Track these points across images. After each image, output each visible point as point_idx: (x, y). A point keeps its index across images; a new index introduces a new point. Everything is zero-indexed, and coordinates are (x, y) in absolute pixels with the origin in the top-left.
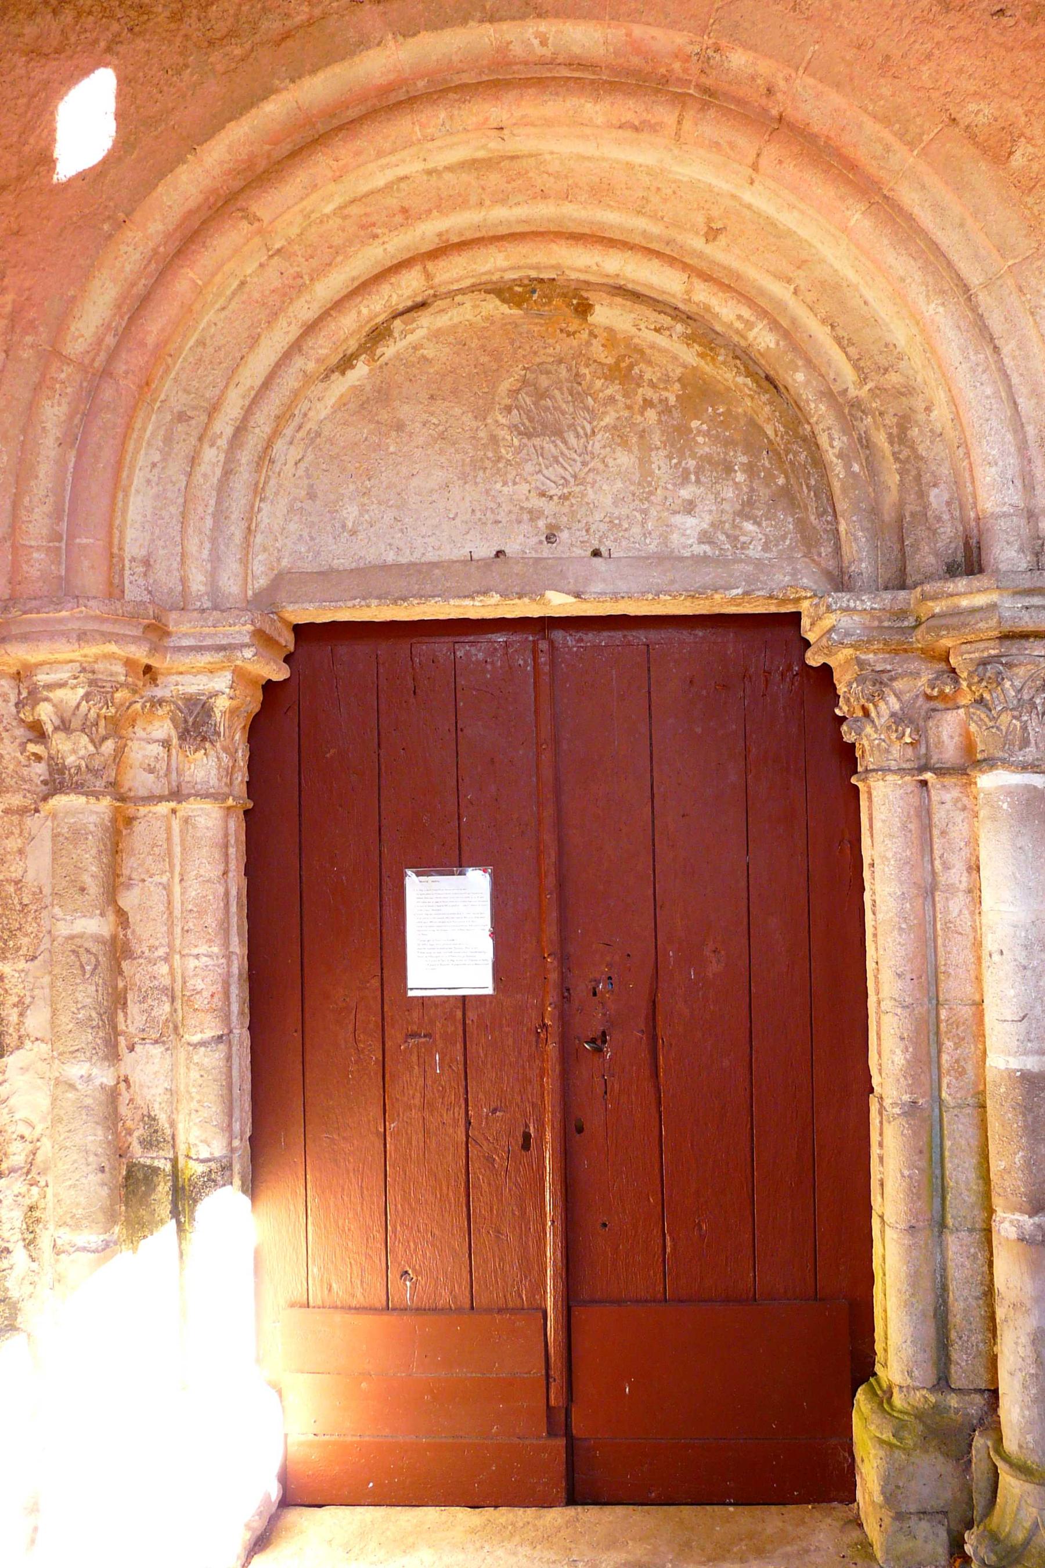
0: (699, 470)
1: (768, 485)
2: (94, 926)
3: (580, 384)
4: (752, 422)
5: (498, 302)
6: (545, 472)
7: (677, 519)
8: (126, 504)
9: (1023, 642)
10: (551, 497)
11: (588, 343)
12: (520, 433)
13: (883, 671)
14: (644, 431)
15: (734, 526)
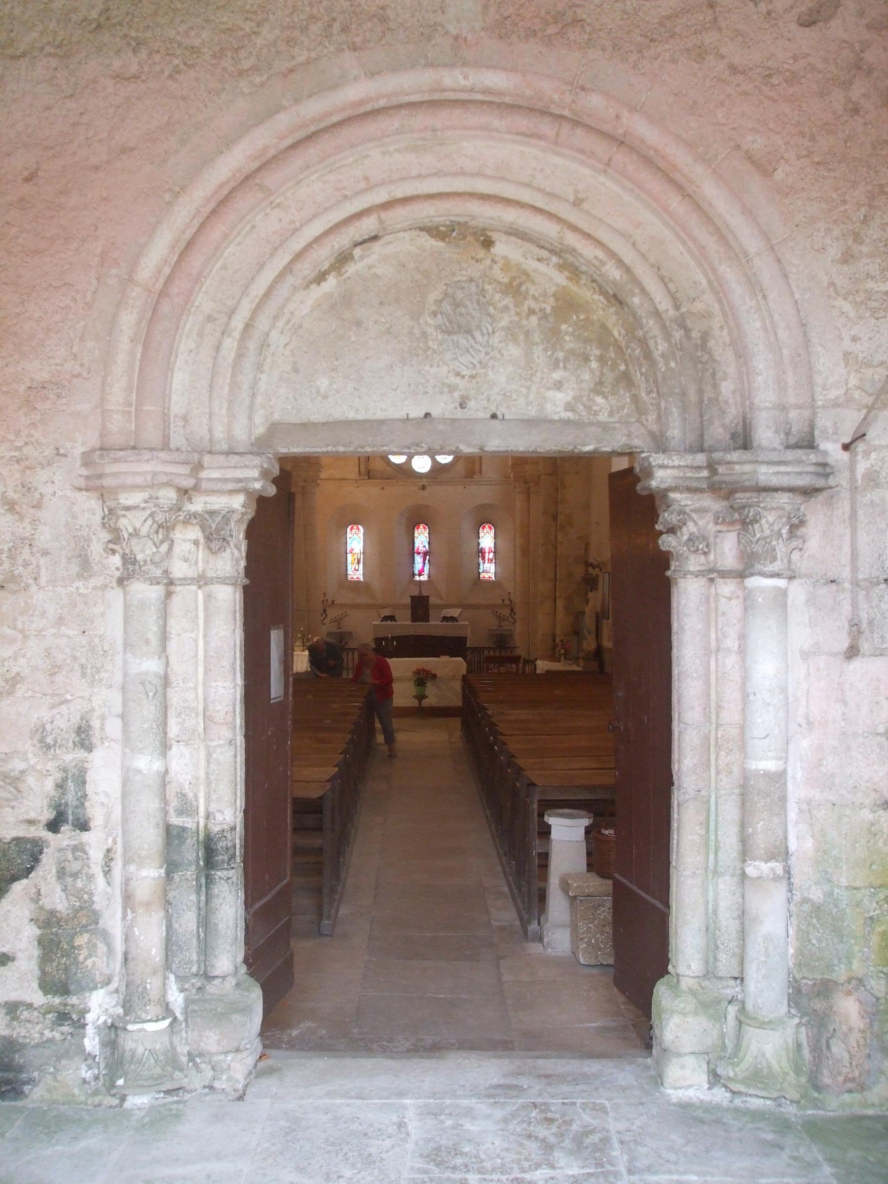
0: (566, 360)
1: (612, 371)
2: (152, 666)
3: (484, 297)
4: (603, 326)
5: (428, 237)
6: (460, 359)
7: (550, 394)
8: (172, 378)
9: (774, 494)
10: (464, 377)
11: (491, 268)
12: (443, 331)
13: (686, 505)
14: (528, 331)
15: (589, 400)
